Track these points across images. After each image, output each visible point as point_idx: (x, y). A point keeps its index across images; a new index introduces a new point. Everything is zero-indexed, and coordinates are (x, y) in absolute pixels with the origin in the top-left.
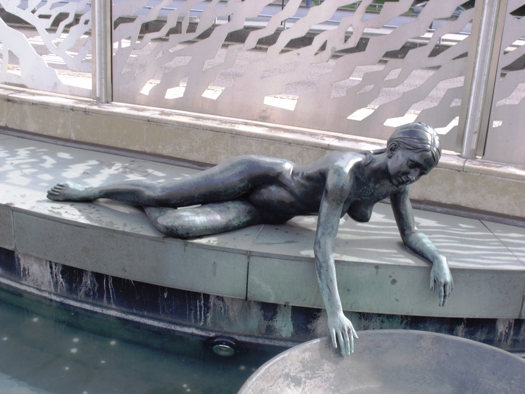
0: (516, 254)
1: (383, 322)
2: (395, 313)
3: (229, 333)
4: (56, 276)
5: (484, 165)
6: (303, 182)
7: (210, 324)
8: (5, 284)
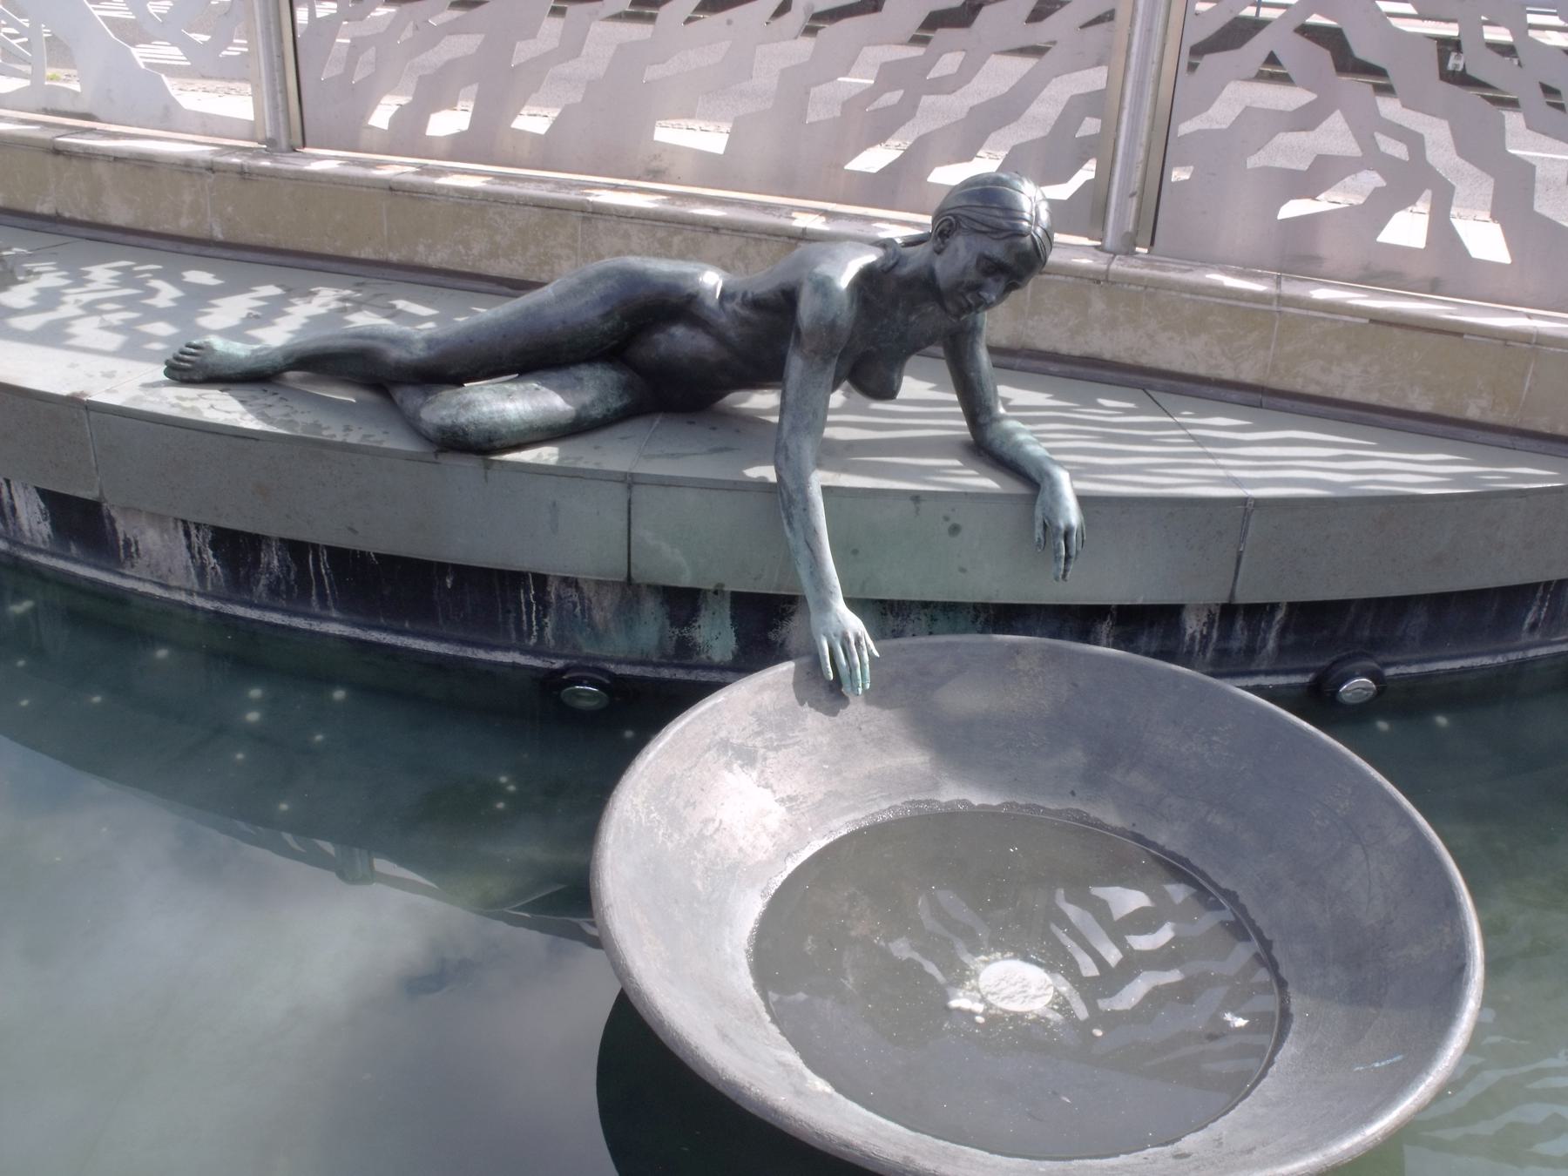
0: (1222, 462)
1: (934, 619)
2: (959, 599)
3: (595, 659)
4: (200, 553)
5: (1153, 267)
6: (745, 312)
7: (552, 643)
8: (86, 579)
